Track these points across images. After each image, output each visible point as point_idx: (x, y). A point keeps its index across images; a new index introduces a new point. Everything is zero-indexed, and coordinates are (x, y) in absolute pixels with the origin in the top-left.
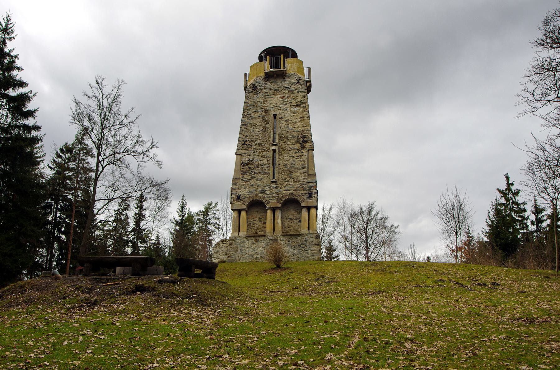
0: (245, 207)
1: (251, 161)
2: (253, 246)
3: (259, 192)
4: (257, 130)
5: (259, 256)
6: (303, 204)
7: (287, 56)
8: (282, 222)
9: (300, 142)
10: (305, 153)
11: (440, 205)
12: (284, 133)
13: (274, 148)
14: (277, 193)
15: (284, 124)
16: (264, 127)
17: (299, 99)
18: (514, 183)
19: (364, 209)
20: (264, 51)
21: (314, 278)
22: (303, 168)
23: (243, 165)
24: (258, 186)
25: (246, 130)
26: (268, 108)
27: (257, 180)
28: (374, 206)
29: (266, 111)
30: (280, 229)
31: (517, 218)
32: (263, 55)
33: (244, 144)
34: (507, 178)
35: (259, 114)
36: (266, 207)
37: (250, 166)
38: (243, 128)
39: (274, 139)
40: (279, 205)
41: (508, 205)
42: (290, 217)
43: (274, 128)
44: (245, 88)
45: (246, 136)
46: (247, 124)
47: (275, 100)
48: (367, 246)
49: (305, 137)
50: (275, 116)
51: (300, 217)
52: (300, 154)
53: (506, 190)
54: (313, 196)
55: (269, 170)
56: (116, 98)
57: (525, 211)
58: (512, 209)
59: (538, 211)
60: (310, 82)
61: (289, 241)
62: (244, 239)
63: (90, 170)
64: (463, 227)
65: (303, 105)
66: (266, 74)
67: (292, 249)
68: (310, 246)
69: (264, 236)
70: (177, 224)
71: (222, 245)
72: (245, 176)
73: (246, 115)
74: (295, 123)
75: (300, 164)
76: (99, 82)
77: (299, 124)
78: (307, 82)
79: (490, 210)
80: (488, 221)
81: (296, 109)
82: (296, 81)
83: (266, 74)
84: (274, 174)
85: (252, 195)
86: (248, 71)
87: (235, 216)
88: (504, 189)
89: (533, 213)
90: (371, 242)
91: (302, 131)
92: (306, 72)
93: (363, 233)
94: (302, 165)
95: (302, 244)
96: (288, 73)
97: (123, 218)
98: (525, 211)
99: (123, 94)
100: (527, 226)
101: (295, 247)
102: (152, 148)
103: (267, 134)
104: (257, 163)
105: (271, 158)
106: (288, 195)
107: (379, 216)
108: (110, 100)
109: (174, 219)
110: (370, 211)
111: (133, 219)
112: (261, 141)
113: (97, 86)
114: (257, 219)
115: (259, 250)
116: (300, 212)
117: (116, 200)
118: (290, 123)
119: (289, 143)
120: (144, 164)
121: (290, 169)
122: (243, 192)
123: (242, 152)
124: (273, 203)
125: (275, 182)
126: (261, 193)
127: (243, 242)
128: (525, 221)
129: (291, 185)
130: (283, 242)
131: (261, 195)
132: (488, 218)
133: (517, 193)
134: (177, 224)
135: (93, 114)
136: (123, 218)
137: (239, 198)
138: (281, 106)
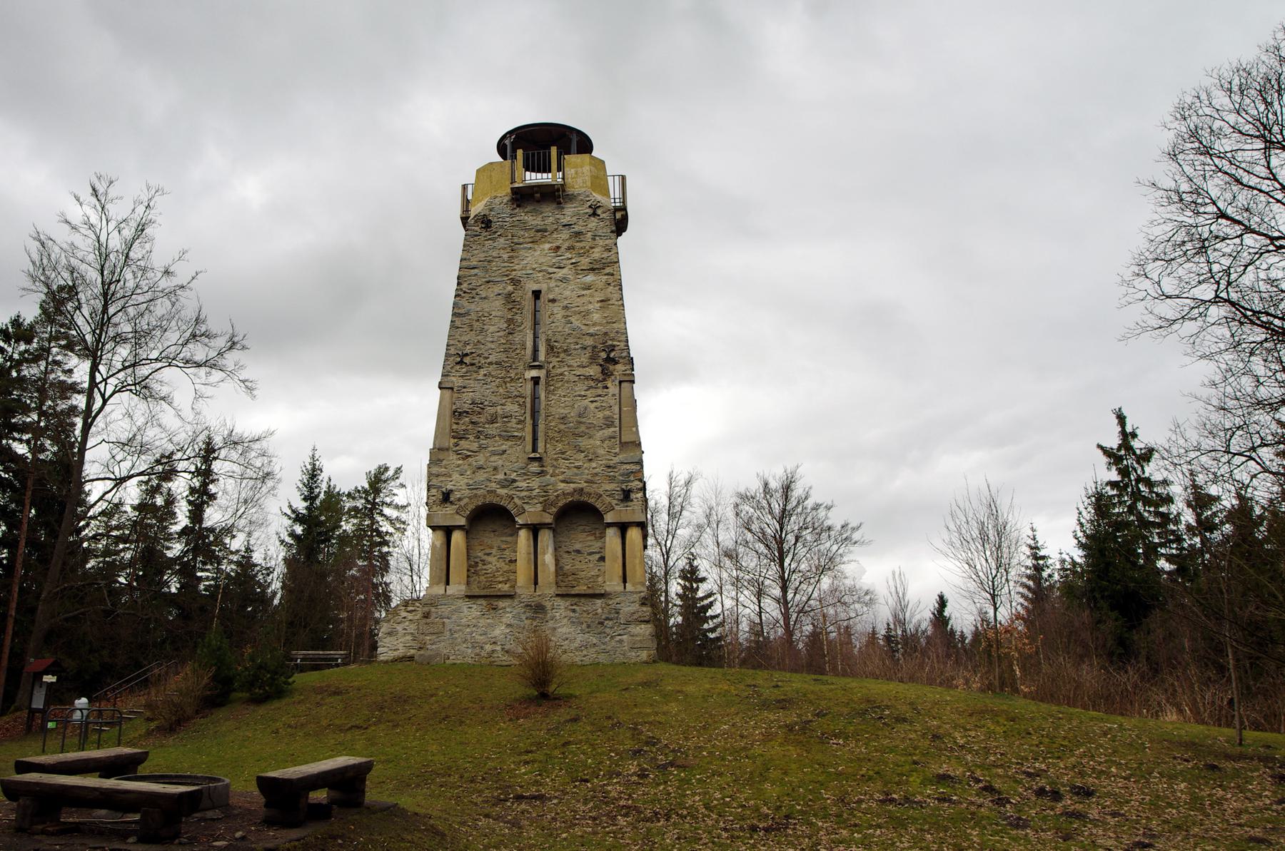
0: (462, 522)
1: (479, 406)
2: (482, 622)
3: (499, 483)
4: (492, 329)
5: (498, 648)
6: (609, 518)
7: (565, 150)
8: (557, 561)
9: (601, 361)
10: (613, 389)
11: (952, 527)
12: (559, 338)
13: (534, 373)
14: (544, 489)
15: (559, 316)
16: (510, 321)
17: (596, 254)
18: (1138, 432)
19: (773, 485)
20: (510, 132)
21: (629, 745)
22: (608, 426)
23: (457, 414)
24: (495, 469)
25: (466, 328)
26: (519, 273)
27: (494, 453)
28: (797, 476)
29: (516, 282)
30: (552, 578)
31: (1151, 519)
32: (507, 142)
33: (461, 362)
34: (1121, 419)
35: (497, 289)
36: (514, 522)
37: (475, 419)
38: (458, 323)
39: (535, 350)
40: (548, 519)
41: (1126, 486)
42: (578, 546)
43: (536, 323)
44: (465, 220)
45: (466, 344)
46: (467, 314)
47: (536, 257)
48: (782, 577)
49: (613, 348)
50: (537, 294)
51: (603, 548)
52: (600, 392)
53: (1119, 449)
54: (633, 496)
55: (523, 429)
56: (141, 229)
57: (1169, 500)
58: (1137, 495)
59: (1200, 501)
60: (624, 209)
61: (574, 611)
62: (460, 603)
63: (74, 388)
64: (1014, 561)
65: (608, 270)
66: (515, 191)
67: (583, 632)
68: (628, 623)
69: (511, 597)
70: (298, 518)
71: (404, 614)
72: (462, 442)
73: (465, 290)
74: (588, 313)
75: (600, 415)
76: (101, 190)
77: (596, 317)
78: (616, 209)
79: (1082, 509)
80: (1080, 534)
81: (590, 278)
82: (590, 211)
83: (515, 191)
84: (535, 440)
85: (479, 492)
86: (471, 179)
87: (438, 544)
88: (1115, 447)
89: (1189, 505)
90: (793, 566)
91: (606, 334)
92: (614, 190)
93: (774, 545)
94: (606, 418)
95: (607, 619)
96: (570, 191)
97: (159, 501)
98: (1169, 500)
99: (159, 219)
100: (1179, 540)
101: (589, 626)
102: (231, 348)
103: (517, 338)
104: (492, 410)
105: (528, 400)
106: (572, 494)
107: (809, 503)
108: (128, 233)
109: (290, 506)
110: (787, 489)
111: (184, 504)
112: (503, 357)
113: (94, 200)
114: (494, 551)
115: (500, 631)
116: (602, 536)
117: (135, 480)
118: (575, 313)
119: (571, 362)
120: (208, 391)
121: (575, 430)
122: (458, 483)
123: (456, 381)
124: (534, 512)
125: (539, 460)
126: (503, 487)
127: (458, 610)
128: (1172, 527)
129: (578, 468)
130: (560, 609)
131: (502, 492)
132: (1078, 528)
133: (1147, 456)
134: (298, 518)
135: (83, 267)
136: (159, 501)
137: (446, 497)
138: (551, 270)
